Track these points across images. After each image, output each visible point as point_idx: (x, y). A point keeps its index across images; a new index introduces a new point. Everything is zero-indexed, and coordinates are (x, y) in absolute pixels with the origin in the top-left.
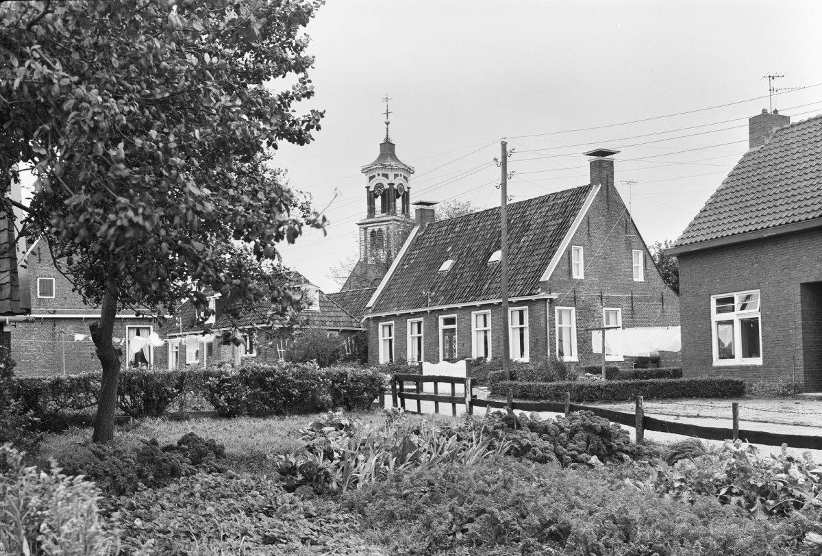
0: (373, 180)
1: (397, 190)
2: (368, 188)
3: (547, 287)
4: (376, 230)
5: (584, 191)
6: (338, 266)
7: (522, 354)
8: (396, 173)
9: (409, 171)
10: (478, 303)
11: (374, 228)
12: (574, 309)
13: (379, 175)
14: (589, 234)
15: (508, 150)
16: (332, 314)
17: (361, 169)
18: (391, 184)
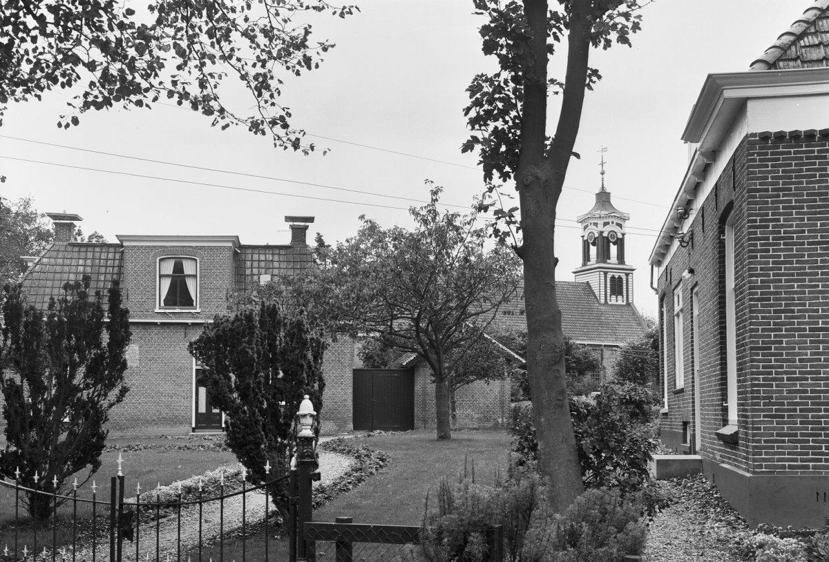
0: (607, 227)
1: (607, 238)
2: (583, 237)
4: (617, 277)
8: (606, 221)
11: (621, 274)
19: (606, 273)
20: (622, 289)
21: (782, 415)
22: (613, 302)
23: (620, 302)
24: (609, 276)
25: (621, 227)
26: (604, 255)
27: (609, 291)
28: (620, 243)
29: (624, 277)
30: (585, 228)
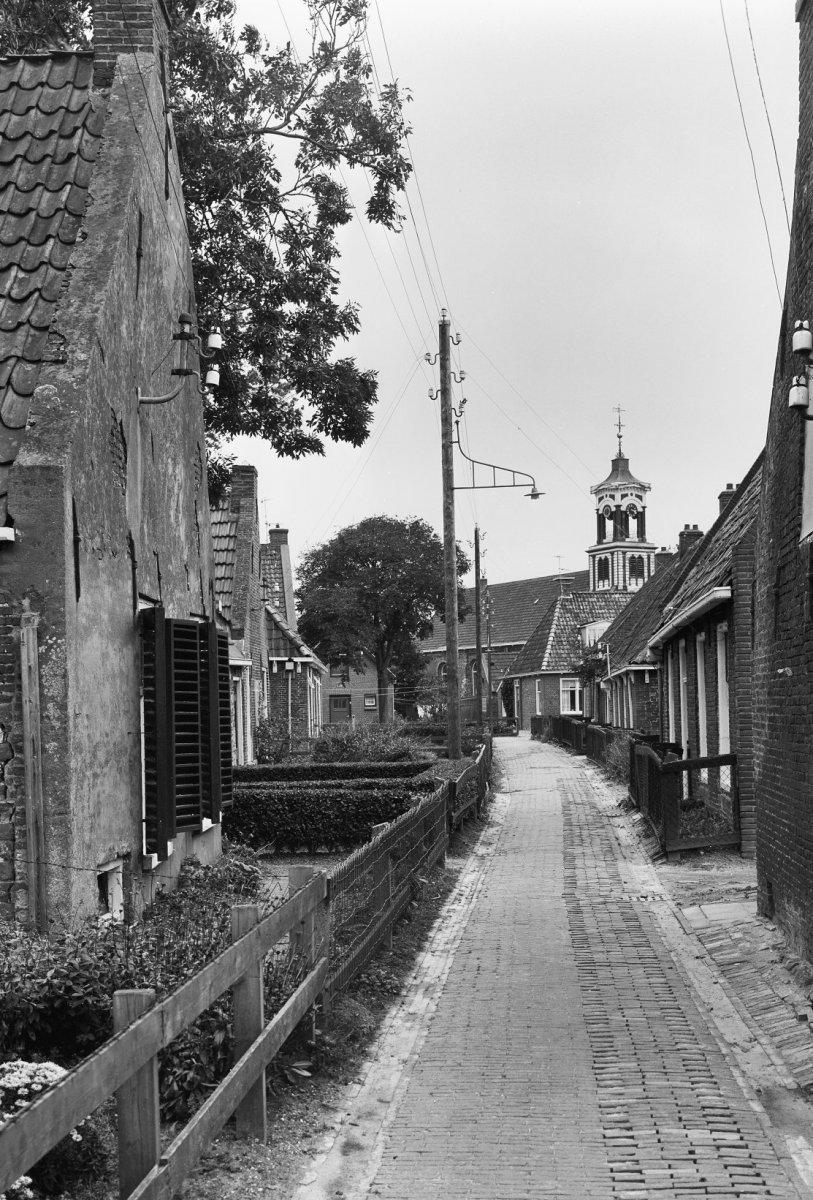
1: (625, 512)
7: (573, 707)
8: (624, 493)
9: (643, 488)
13: (632, 494)
18: (618, 507)
19: (624, 553)
20: (599, 572)
21: (192, 726)
22: (601, 588)
23: (607, 587)
24: (597, 559)
26: (621, 532)
27: (627, 573)
28: (641, 517)
29: (609, 556)
30: (601, 499)
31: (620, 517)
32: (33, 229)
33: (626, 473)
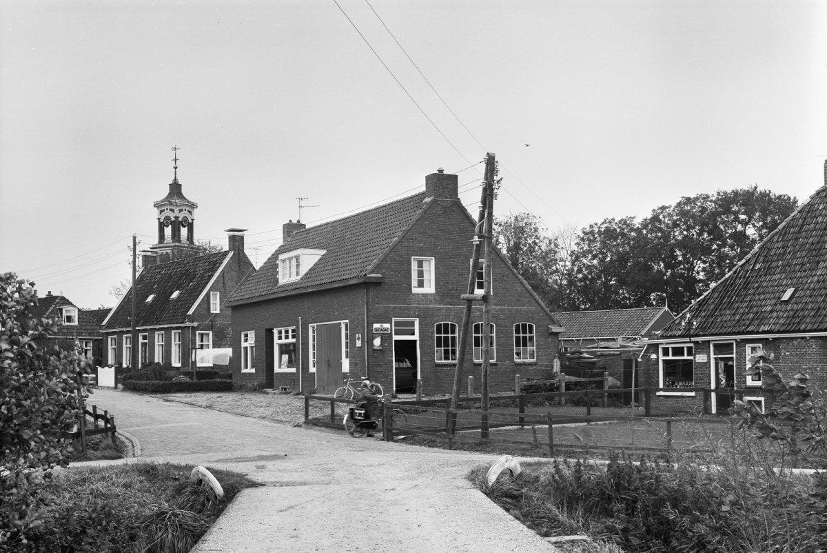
2: (159, 219)
3: (192, 319)
5: (226, 253)
6: (120, 286)
8: (182, 208)
9: (193, 206)
10: (157, 327)
12: (211, 332)
13: (167, 209)
14: (224, 284)
15: (137, 241)
16: (88, 327)
17: (153, 204)
18: (177, 218)
25: (191, 214)
30: (161, 212)
31: (176, 225)
32: (338, 429)
33: (181, 196)
